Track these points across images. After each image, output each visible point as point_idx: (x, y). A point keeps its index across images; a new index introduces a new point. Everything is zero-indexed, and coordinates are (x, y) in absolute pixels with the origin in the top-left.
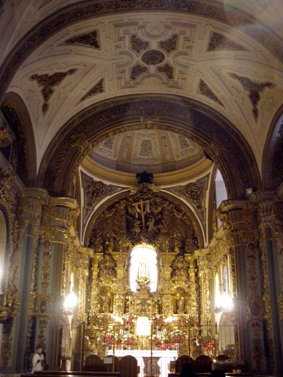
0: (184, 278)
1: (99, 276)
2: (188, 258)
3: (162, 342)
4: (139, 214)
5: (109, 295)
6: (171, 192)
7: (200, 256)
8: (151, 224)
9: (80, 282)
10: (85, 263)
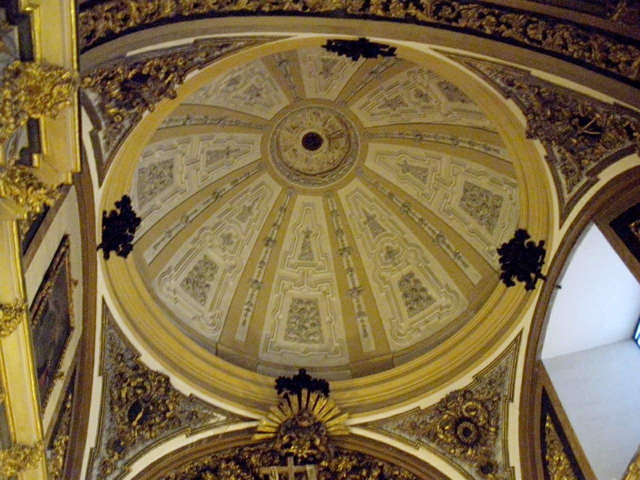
6: (389, 435)
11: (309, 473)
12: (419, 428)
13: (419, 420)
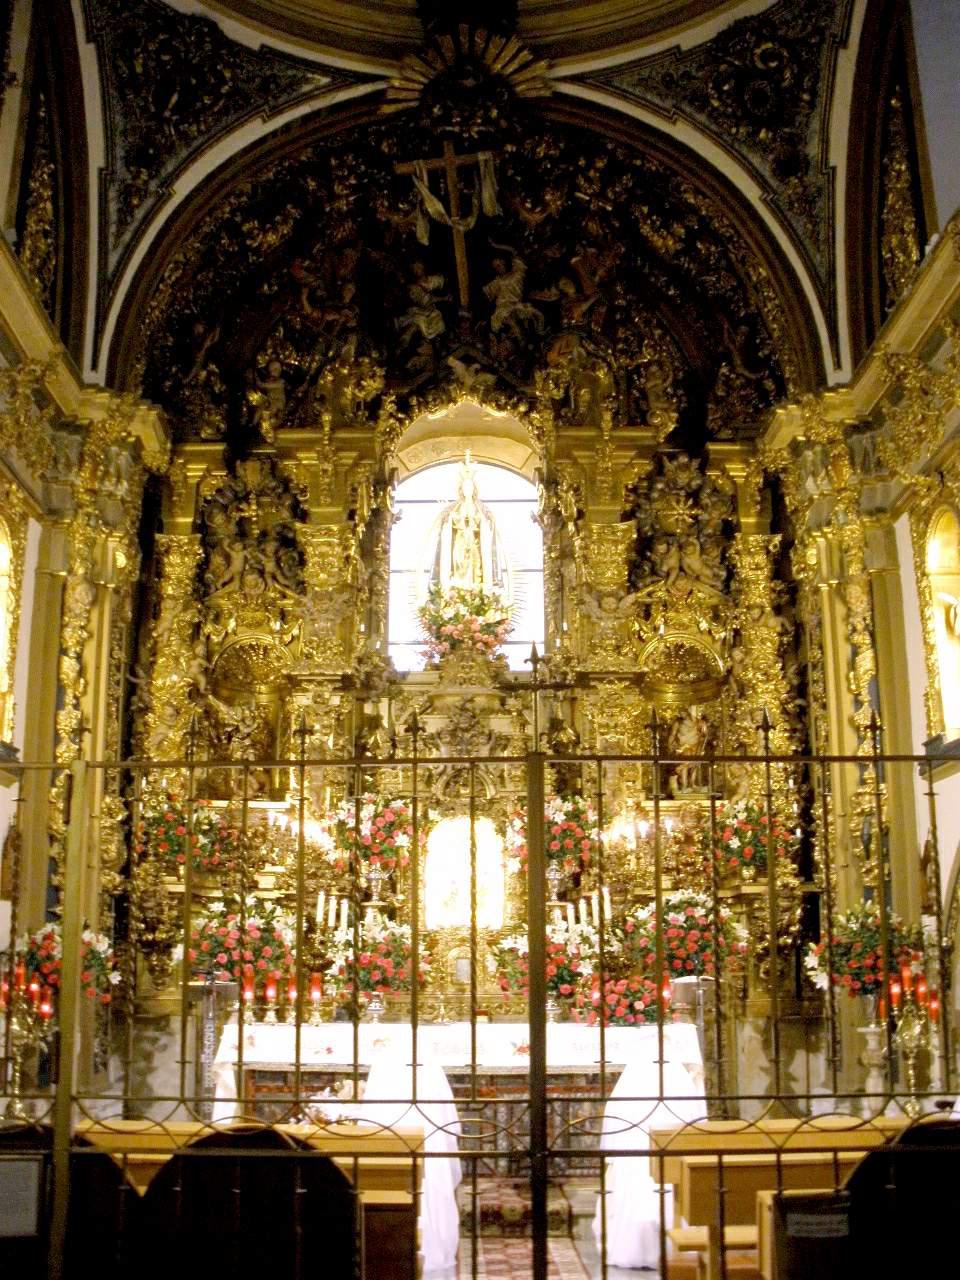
0: (705, 594)
1: (201, 586)
2: (724, 471)
3: (586, 969)
4: (438, 230)
5: (264, 699)
6: (623, 95)
7: (809, 444)
8: (507, 291)
9: (70, 601)
10: (111, 495)
11: (482, 164)
12: (678, 86)
13: (675, 72)
